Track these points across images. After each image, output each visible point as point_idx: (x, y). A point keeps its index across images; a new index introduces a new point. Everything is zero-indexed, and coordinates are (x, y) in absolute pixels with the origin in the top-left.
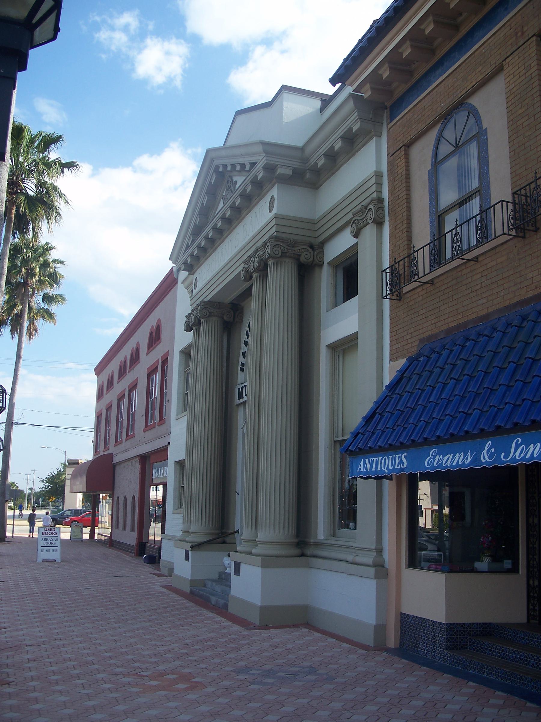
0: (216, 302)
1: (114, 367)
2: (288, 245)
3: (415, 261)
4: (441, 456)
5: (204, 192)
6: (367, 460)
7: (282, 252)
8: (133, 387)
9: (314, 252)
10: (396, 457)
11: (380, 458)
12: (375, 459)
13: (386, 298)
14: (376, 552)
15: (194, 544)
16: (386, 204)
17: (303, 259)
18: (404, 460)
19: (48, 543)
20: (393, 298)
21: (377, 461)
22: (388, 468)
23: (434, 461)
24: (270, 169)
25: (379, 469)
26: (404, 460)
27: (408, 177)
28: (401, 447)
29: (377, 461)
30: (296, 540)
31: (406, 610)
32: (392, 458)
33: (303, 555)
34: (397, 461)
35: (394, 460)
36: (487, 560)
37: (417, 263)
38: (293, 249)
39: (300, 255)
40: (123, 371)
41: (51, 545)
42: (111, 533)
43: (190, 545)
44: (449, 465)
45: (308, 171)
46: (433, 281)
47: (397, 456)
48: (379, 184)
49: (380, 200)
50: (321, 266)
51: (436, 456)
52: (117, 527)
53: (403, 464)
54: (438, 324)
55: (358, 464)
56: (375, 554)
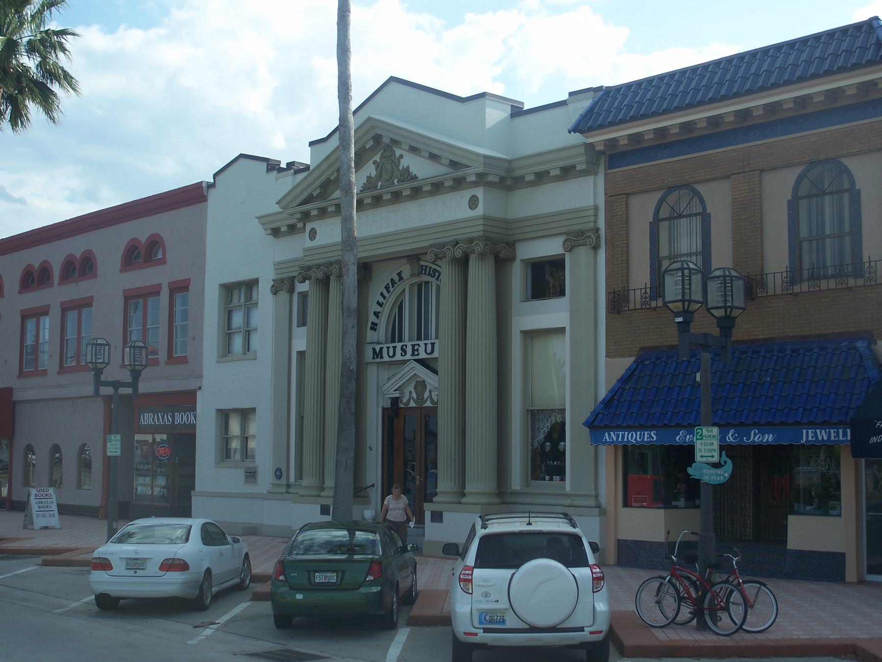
16: (602, 233)
22: (636, 439)
28: (652, 427)
30: (497, 491)
31: (623, 536)
36: (682, 500)
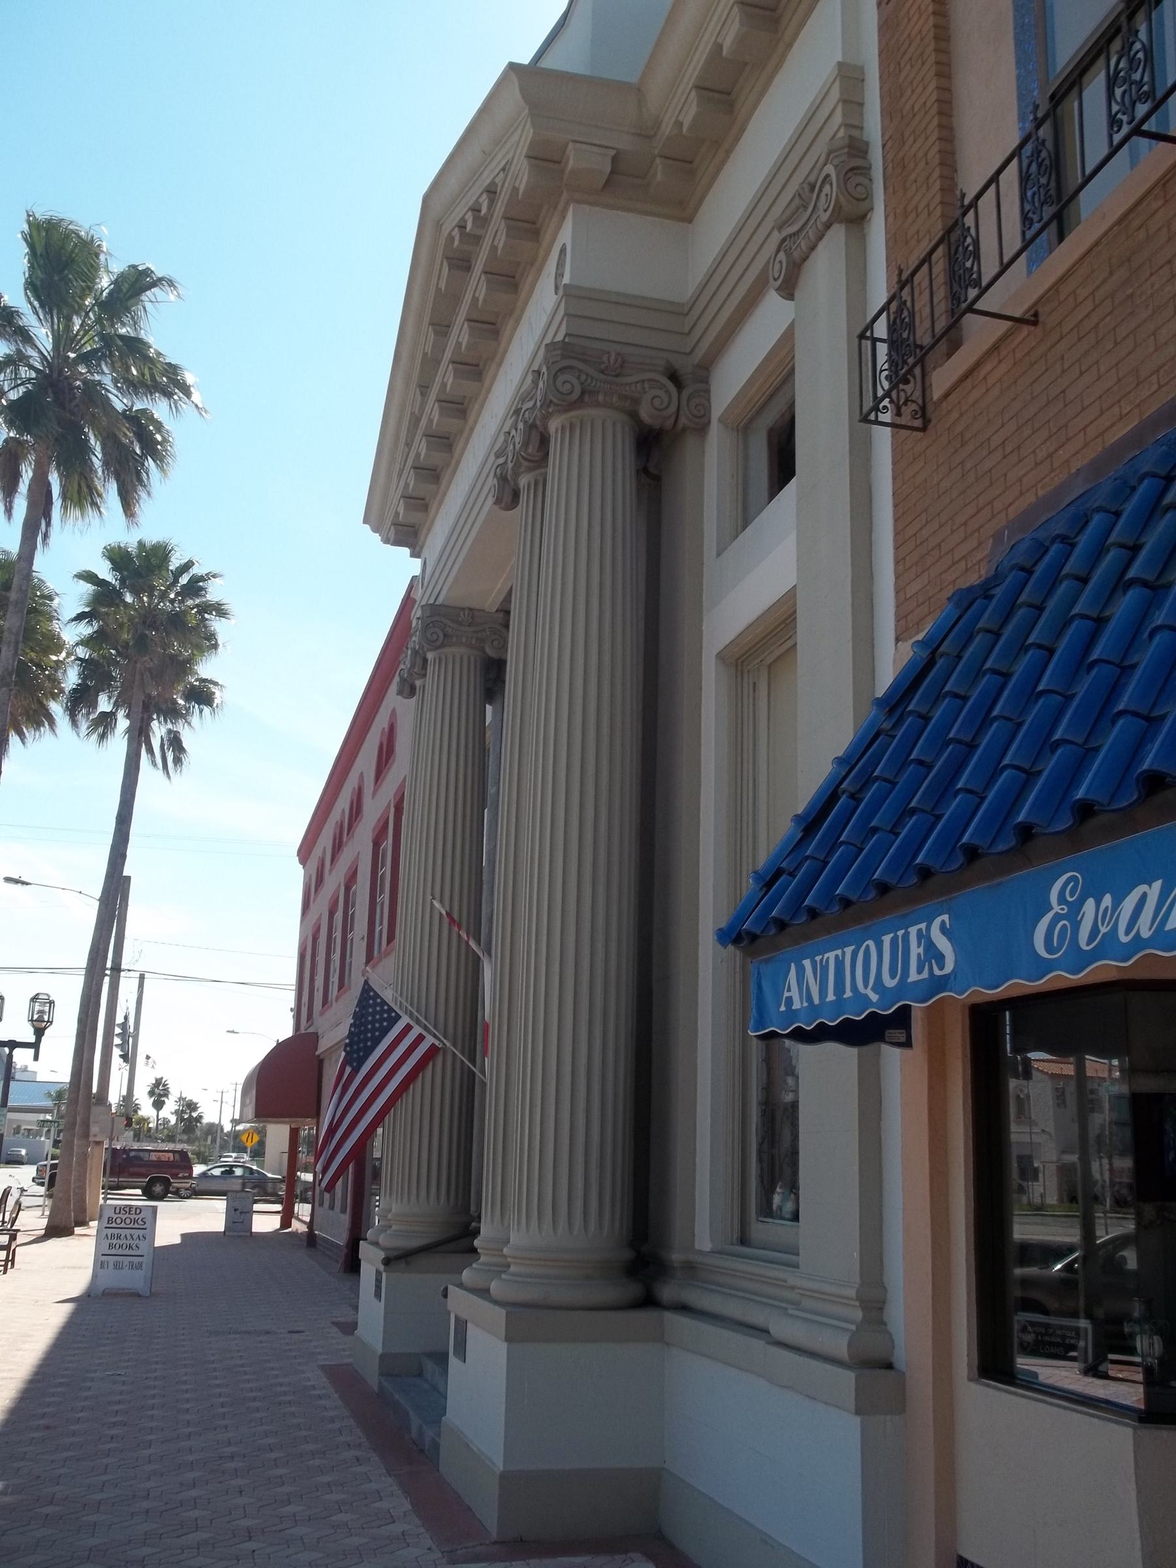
0: (463, 609)
1: (326, 840)
2: (602, 372)
3: (969, 240)
4: (1107, 900)
5: (427, 320)
6: (807, 963)
7: (583, 393)
8: (351, 879)
9: (679, 393)
10: (906, 936)
11: (849, 950)
12: (831, 956)
13: (877, 422)
14: (863, 1309)
15: (393, 1254)
17: (646, 414)
18: (943, 944)
19: (121, 1246)
20: (899, 421)
21: (839, 964)
22: (879, 986)
23: (1076, 926)
24: (546, 158)
25: (848, 994)
26: (943, 944)
27: (943, 35)
29: (839, 964)
32: (894, 942)
33: (648, 1301)
34: (915, 950)
35: (900, 953)
37: (976, 242)
38: (619, 380)
39: (636, 401)
40: (338, 846)
41: (127, 1252)
42: (312, 1215)
43: (382, 1255)
44: (1146, 934)
45: (658, 161)
46: (1036, 315)
47: (913, 931)
48: (853, 103)
49: (857, 148)
50: (702, 429)
51: (1081, 901)
52: (321, 1204)
53: (940, 958)
54: (1063, 454)
55: (779, 985)
56: (859, 1315)
